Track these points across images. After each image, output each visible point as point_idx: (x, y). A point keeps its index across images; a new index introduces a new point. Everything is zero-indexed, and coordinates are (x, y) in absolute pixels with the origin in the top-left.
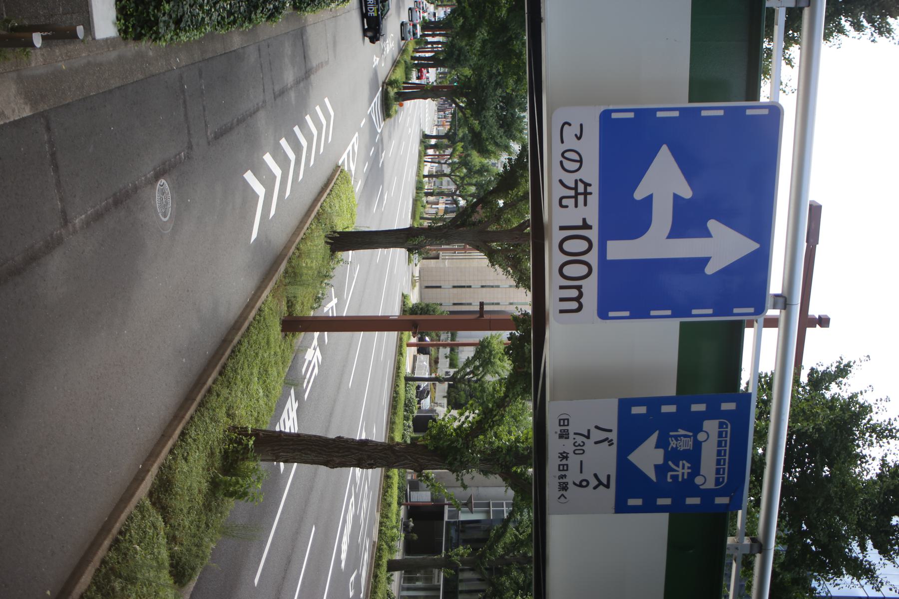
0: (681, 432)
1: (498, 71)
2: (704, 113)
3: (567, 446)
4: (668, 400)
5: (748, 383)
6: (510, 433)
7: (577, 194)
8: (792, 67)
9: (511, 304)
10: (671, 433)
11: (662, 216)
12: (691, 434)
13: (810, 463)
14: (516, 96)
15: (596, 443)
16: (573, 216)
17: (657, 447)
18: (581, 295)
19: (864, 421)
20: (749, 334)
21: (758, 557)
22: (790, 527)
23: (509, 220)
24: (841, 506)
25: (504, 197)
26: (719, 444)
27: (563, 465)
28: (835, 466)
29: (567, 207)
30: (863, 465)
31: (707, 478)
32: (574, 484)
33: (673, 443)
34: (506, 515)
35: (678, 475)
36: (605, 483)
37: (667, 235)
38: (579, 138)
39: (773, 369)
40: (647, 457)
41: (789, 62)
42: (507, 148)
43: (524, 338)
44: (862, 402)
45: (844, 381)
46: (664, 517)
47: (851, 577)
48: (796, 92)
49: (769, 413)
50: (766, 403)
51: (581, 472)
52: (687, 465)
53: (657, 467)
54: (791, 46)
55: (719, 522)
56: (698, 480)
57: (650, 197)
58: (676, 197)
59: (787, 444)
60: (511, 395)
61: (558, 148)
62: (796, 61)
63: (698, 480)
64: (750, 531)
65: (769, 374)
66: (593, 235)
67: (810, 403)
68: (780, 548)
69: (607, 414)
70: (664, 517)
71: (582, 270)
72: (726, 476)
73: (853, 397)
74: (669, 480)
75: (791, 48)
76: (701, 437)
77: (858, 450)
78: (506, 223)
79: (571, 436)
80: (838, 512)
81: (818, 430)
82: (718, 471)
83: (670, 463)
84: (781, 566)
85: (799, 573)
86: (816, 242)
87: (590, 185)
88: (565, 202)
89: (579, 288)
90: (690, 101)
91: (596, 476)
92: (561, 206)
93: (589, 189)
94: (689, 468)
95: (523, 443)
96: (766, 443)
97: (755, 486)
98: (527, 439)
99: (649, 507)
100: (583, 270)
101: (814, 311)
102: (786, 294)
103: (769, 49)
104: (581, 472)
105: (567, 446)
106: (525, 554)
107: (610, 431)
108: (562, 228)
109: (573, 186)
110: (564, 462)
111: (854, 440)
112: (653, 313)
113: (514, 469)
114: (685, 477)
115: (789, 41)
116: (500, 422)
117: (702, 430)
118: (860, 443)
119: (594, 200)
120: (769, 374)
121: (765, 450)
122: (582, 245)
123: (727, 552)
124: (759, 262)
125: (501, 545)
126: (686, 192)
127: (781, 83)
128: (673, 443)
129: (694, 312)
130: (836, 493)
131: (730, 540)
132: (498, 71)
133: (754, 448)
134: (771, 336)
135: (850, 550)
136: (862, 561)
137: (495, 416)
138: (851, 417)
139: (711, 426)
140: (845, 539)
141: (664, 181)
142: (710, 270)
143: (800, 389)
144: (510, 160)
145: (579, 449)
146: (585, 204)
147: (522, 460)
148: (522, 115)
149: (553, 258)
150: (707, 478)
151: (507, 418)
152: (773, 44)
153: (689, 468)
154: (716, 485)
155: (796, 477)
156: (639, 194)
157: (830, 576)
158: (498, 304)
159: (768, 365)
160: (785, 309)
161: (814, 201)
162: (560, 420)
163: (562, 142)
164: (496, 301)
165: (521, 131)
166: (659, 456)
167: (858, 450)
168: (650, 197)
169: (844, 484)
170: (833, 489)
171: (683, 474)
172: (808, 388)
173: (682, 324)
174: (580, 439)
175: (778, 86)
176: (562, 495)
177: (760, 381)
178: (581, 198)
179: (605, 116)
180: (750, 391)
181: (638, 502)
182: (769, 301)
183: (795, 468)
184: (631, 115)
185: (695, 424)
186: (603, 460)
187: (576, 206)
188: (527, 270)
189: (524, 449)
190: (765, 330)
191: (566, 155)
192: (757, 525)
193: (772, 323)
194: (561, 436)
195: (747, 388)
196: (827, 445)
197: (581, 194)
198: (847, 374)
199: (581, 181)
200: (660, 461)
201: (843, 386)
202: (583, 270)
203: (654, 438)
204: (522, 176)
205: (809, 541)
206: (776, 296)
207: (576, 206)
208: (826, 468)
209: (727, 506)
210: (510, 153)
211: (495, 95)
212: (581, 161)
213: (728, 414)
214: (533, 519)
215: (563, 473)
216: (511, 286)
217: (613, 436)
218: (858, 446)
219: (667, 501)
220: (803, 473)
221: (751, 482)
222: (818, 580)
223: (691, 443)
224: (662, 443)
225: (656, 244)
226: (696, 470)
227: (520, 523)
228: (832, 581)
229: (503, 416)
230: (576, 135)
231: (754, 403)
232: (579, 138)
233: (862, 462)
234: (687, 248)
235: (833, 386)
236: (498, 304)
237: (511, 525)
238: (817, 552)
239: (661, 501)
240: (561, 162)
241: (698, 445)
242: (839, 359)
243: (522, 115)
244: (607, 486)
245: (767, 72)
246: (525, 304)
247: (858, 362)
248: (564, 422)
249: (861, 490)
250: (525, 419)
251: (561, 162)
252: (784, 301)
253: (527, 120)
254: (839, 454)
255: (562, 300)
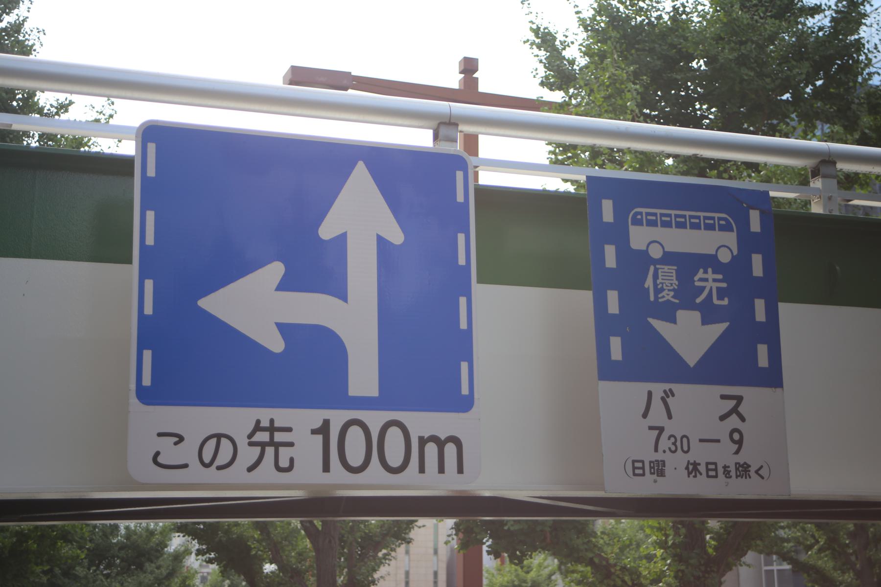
0: (649, 283)
1: (45, 573)
2: (150, 241)
3: (676, 463)
4: (600, 304)
5: (565, 181)
6: (650, 558)
7: (272, 443)
8: (71, 103)
9: (436, 552)
10: (652, 298)
11: (311, 308)
12: (652, 268)
13: (687, 88)
14: (91, 541)
15: (670, 417)
16: (306, 450)
17: (673, 321)
18: (434, 439)
19: (622, 9)
20: (488, 178)
21: (840, 166)
22: (789, 117)
23: (300, 554)
24: (753, 42)
25: (261, 561)
26: (667, 225)
27: (708, 470)
28: (691, 51)
29: (292, 460)
30: (687, 10)
31: (721, 243)
32: (737, 452)
33: (667, 296)
34: (786, 567)
35: (718, 289)
36: (734, 402)
37: (341, 302)
38: (181, 439)
39: (544, 143)
40: (690, 336)
41: (63, 107)
42: (179, 557)
43: (496, 531)
44: (592, 12)
45: (560, 37)
46: (784, 308)
47: (864, 28)
48: (113, 99)
49: (612, 149)
50: (596, 153)
51: (718, 441)
52: (701, 274)
53: (705, 322)
54: (37, 103)
55: (791, 229)
56: (725, 257)
57: (281, 327)
58: (281, 287)
59: (659, 123)
60: (590, 555)
61: (196, 474)
62: (62, 97)
63: (725, 257)
64: (802, 179)
65: (551, 148)
66: (338, 418)
67: (595, 87)
68: (818, 133)
69: (623, 398)
70: (784, 308)
71: (394, 436)
72: (716, 215)
73: (583, 23)
74: (726, 302)
75: (41, 104)
76: (656, 253)
77: (666, 17)
78: (305, 560)
79: (659, 456)
80: (761, 48)
81: (636, 75)
82: (710, 227)
83: (698, 300)
84: (850, 129)
85: (860, 104)
86: (348, 74)
87: (258, 422)
88: (284, 463)
89: (423, 442)
90: (129, 261)
91: (723, 418)
92: (290, 469)
93: (265, 423)
94: (706, 272)
95: (667, 536)
96: (659, 154)
97: (726, 171)
98: (660, 529)
99: (770, 333)
100: (394, 433)
101: (453, 80)
102: (435, 124)
103: (41, 136)
104: (718, 441)
105: (676, 463)
106: (853, 535)
107: (650, 394)
108: (326, 468)
109: (258, 450)
110: (702, 468)
111: (650, 23)
112: (463, 325)
113: (710, 551)
114: (720, 277)
115: (29, 106)
116: (635, 573)
117: (646, 252)
118: (655, 14)
119: (282, 416)
120: (551, 148)
121: (668, 156)
122: (355, 435)
123: (836, 213)
124: (383, 162)
125: (837, 575)
126: (276, 270)
127: (97, 121)
128: (667, 296)
129: (462, 261)
130: (732, 50)
131: (817, 208)
132: (45, 573)
133: (666, 171)
134: (491, 146)
135: (821, 29)
136: (836, 12)
137: (624, 581)
138: (615, 28)
139: (639, 237)
140: (802, 36)
141: (255, 305)
142: (396, 236)
143: (574, 102)
144: (199, 552)
145: (681, 444)
146: (289, 430)
147: (695, 538)
148: (123, 531)
149: (375, 483)
150: (721, 243)
151: (627, 561)
152: (32, 132)
153: (706, 272)
154: (732, 230)
155: (708, 109)
156: (276, 344)
157: (862, 58)
158: (436, 574)
159: (537, 150)
160: (457, 125)
161: (284, 77)
162: (635, 475)
163: (185, 466)
164: (431, 578)
165: (152, 533)
166: (689, 318)
167: (666, 17)
168: (281, 327)
169: (719, 39)
170: (727, 54)
171: (715, 280)
172: (571, 91)
173: (480, 281)
174: (665, 443)
175: (100, 125)
176: (757, 472)
177: (562, 163)
178: (279, 437)
179: (146, 396)
180: (582, 178)
181: (762, 351)
182: (445, 148)
183: (695, 110)
184: (147, 355)
185: (636, 263)
186: (697, 407)
187: (291, 444)
188: (382, 525)
189: (677, 534)
190: (481, 154)
191: (207, 460)
192: (786, 167)
193: (471, 143)
194: (661, 473)
195: (573, 182)
196: (659, 63)
197: (272, 437)
198: (549, 34)
199: (250, 436)
200: (696, 316)
201: (569, 40)
202: (394, 433)
203: (659, 325)
204: (227, 532)
205: (808, 90)
206: (436, 137)
207: (291, 444)
208: (694, 64)
209: (762, 213)
210: (187, 552)
211: (86, 577)
212: (219, 437)
213: (620, 212)
214: (790, 521)
215: (721, 471)
216: (407, 552)
217: (658, 389)
218: (659, 18)
219: (760, 305)
220: (702, 99)
221: (719, 176)
222: (870, 75)
223: (666, 268)
224: (668, 314)
225: (354, 319)
226: (709, 261)
227: (798, 542)
228: (870, 56)
229: (624, 569)
230: (176, 444)
231: (596, 172)
232: (181, 439)
233: (684, 12)
234: (362, 272)
235: (567, 54)
236: (436, 574)
237: (803, 557)
238: (827, 77)
239: (760, 315)
240: (219, 468)
241: (669, 258)
242: (528, 45)
243: (123, 531)
244: (739, 399)
245: (79, 142)
246: (436, 528)
247: (532, 17)
248: (637, 468)
249: (728, 13)
250: (624, 531)
251: (219, 468)
252: (444, 126)
253: (132, 524)
254: (673, 46)
255: (441, 470)
